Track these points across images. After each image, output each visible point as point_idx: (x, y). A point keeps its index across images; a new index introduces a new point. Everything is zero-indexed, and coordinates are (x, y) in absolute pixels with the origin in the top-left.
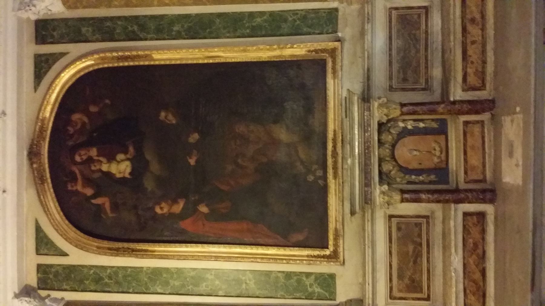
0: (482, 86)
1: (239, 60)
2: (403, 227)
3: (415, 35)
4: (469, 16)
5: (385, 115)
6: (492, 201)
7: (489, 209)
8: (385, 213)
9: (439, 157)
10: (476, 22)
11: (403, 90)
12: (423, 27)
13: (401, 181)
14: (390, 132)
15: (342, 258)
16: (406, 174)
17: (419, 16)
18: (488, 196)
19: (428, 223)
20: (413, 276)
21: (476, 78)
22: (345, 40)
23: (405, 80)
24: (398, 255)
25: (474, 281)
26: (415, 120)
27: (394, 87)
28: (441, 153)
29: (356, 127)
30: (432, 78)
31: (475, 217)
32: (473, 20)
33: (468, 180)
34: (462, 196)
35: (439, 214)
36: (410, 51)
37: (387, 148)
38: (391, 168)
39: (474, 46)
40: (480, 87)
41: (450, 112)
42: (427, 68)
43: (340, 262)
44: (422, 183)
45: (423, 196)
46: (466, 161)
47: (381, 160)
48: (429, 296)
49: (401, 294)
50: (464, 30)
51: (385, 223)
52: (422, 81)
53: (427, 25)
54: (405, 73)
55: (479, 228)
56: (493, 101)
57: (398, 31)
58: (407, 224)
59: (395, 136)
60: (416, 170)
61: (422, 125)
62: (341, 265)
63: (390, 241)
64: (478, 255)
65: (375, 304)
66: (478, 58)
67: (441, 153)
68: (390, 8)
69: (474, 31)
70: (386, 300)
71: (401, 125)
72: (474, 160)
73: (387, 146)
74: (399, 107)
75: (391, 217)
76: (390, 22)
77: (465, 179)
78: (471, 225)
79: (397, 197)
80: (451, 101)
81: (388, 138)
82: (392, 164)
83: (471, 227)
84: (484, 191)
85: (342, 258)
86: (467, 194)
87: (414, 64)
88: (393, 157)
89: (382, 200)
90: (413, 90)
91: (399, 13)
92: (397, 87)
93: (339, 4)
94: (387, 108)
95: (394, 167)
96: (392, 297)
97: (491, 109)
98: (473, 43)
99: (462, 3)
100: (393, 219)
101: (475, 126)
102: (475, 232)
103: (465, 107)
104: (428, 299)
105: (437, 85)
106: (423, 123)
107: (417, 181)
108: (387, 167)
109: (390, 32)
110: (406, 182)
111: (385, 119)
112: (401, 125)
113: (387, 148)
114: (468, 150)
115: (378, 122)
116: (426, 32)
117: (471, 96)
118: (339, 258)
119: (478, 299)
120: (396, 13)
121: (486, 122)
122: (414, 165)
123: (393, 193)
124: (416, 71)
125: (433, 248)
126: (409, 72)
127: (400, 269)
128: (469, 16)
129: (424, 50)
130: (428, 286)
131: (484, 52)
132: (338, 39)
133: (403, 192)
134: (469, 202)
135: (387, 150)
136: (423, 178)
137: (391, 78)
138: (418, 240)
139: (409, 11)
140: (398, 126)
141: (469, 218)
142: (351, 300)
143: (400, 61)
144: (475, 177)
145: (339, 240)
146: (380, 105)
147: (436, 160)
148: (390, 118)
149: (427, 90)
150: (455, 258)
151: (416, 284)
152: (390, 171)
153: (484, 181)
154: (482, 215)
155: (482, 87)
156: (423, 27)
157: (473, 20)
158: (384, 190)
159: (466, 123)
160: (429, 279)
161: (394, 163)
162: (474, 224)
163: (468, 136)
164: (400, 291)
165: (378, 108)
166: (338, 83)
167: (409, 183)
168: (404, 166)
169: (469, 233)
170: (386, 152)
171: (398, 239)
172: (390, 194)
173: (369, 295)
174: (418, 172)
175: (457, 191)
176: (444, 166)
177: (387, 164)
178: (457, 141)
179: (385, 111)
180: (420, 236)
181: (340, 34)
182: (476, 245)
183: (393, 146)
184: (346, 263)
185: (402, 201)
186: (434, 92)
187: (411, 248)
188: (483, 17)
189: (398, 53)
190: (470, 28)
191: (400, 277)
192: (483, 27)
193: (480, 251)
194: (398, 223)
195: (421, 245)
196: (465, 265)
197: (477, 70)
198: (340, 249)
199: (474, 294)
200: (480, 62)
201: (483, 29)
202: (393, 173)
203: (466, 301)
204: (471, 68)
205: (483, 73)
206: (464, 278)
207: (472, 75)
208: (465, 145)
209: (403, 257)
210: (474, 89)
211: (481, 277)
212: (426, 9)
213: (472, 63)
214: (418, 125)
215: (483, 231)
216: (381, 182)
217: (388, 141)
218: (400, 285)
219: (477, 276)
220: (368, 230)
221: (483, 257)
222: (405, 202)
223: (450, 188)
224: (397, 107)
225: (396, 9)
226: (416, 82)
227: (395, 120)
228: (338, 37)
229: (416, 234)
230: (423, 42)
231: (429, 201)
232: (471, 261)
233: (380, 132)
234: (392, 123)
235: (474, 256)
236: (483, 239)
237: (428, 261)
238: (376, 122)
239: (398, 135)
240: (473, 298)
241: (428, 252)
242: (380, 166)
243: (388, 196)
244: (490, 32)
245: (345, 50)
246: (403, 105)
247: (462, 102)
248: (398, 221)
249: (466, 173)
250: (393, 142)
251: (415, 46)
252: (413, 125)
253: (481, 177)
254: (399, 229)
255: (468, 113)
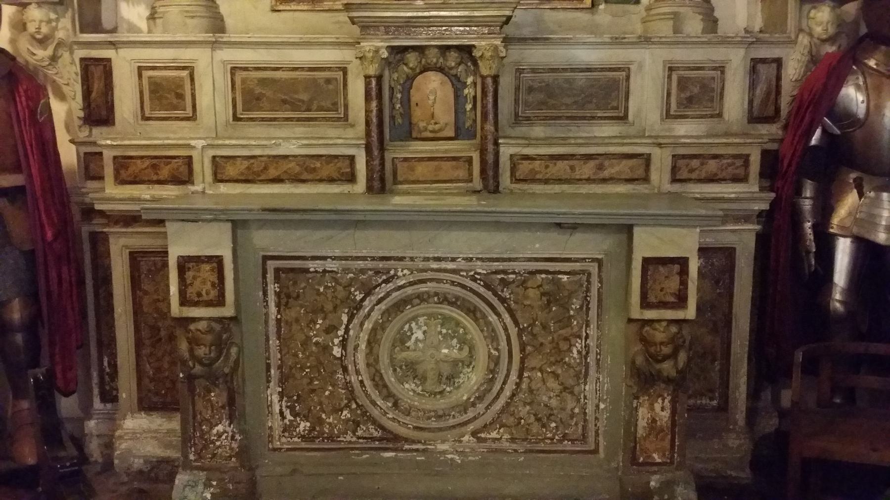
0: (516, 180)
1: (836, 256)
2: (331, 87)
3: (591, 102)
4: (607, 163)
5: (482, 55)
6: (370, 189)
7: (361, 185)
8: (349, 62)
9: (426, 129)
10: (598, 171)
11: (517, 89)
12: (600, 114)
13: (394, 80)
14: (459, 64)
15: (281, 8)
16: (403, 85)
17: (617, 108)
18: (376, 184)
19: (339, 119)
20: (265, 98)
21: (527, 172)
22: (593, 14)
23: (530, 90)
24: (292, 79)
25: (266, 168)
26: (475, 97)
27: (522, 75)
28: (431, 132)
29: (466, 13)
30: (531, 125)
31: (348, 170)
32: (600, 168)
33: (396, 161)
34: (376, 153)
35: (350, 133)
36: (569, 96)
37: (438, 61)
38: (411, 65)
39: (568, 168)
40: (515, 176)
41: (484, 138)
42: (546, 118)
43: (276, 5)
44: (393, 108)
45: (374, 104)
46: (421, 159)
47: (420, 50)
48: (240, 119)
49: (240, 83)
50: (589, 157)
51: (335, 62)
52: (529, 113)
53: (601, 118)
54: (540, 90)
55: (335, 175)
56: (496, 190)
57: (598, 80)
58: (337, 92)
59: (453, 72)
60: (409, 100)
61: (469, 107)
62: (272, 7)
63: (311, 69)
64: (300, 173)
65: (224, 46)
66: (553, 174)
67: (431, 132)
68: (629, 69)
69: (587, 170)
70: (230, 62)
71: (470, 80)
72: (421, 170)
73: (441, 60)
74: (493, 72)
75: (345, 71)
76: (611, 70)
77: (397, 158)
78: (339, 165)
79: (372, 70)
80: (498, 140)
81: (452, 59)
82: (417, 67)
83: (335, 165)
84: (382, 180)
85: (281, 8)
86: (378, 159)
87: (552, 102)
88: (425, 69)
89: (367, 49)
90: (516, 101)
91: (621, 82)
92: (521, 79)
93: (645, 6)
94: (491, 56)
95: (411, 69)
96: (234, 70)
97: (486, 187)
98: (572, 168)
99: (623, 154)
100: (341, 73)
101: (467, 172)
102: (328, 170)
103: (490, 158)
104: (236, 118)
105: (522, 130)
106: (471, 109)
107: (394, 100)
108: (412, 58)
109: (595, 70)
110: (393, 86)
111: (477, 53)
112: (470, 80)
113: (438, 61)
114: (436, 163)
115: (474, 46)
116: (593, 118)
117: (505, 165)
118: (281, 4)
119: (242, 174)
120: (621, 77)
121: (470, 184)
122: (415, 96)
123: (377, 65)
124: (542, 104)
125: (304, 126)
126: (541, 96)
127: (274, 81)
128: (607, 163)
129: (569, 115)
130: (253, 118)
131: (560, 181)
132: (595, 3)
133: (379, 78)
134: (367, 162)
135: (435, 60)
136: (398, 108)
137: (534, 71)
138: (315, 107)
139: (622, 95)
140: (467, 76)
141: (348, 162)
142: (222, 20)
143: (556, 82)
144: (399, 172)
145: (307, 5)
146: (496, 48)
147: (422, 125)
148: (479, 62)
149: (515, 120)
150: (294, 145)
151: (255, 102)
152: (406, 64)
153: (396, 182)
154: (351, 178)
155: (516, 180)
156: (600, 114)
157: (600, 168)
158: (381, 52)
159: (470, 161)
160: (263, 119)
161: (418, 71)
162: (340, 168)
163: (454, 163)
164: (244, 81)
165: (492, 45)
166: (533, 4)
167: (392, 89)
168: (415, 83)
169: (328, 163)
170: (433, 57)
171: (315, 80)
172: (375, 61)
173: (235, 37)
174: (407, 101)
175: (382, 149)
176: (414, 135)
177: (417, 59)
178: (446, 151)
179: (488, 54)
180: (321, 109)
181: (602, 7)
182: (314, 170)
183: (441, 70)
184: (276, 14)
185: (367, 77)
186: (512, 127)
187: (305, 97)
188: (604, 181)
189: (567, 81)
190: (592, 164)
191: (263, 82)
192: (592, 180)
193: (305, 176)
194: (336, 79)
195: (309, 110)
196: (286, 157)
197: (537, 173)
198: (294, 5)
199: (248, 168)
200: (547, 176)
201: (589, 180)
202: (405, 68)
203: (238, 159)
204: (540, 165)
205: (534, 181)
206: (269, 156)
207: (531, 167)
208: (441, 159)
209: (292, 85)
210: (513, 169)
211: (271, 178)
212: (624, 118)
213: (547, 167)
214: (469, 101)
215: (331, 180)
216: (392, 49)
217: (447, 60)
218: (251, 81)
219: (273, 173)
220: (325, 37)
221: (298, 180)
222: (365, 81)
223: (385, 143)
224: (493, 71)
225: (628, 78)
226: (527, 104)
227: (476, 71)
228: (599, 5)
229: (323, 104)
230: (581, 113)
231: (368, 112)
232: (292, 165)
233: (459, 48)
234: (472, 68)
235: (297, 169)
236: (321, 181)
237: (287, 119)
238: (473, 43)
239: (456, 76)
240: (243, 167)
241: (299, 119)
242: (414, 48)
243: (373, 57)
244: (585, 189)
245: (579, 14)
246: (496, 78)
247: (497, 154)
248: (338, 79)
249: (406, 159)
250: (446, 69)
251: (575, 102)
252: (468, 96)
253: (400, 178)
254: (328, 81)
255: (483, 162)
